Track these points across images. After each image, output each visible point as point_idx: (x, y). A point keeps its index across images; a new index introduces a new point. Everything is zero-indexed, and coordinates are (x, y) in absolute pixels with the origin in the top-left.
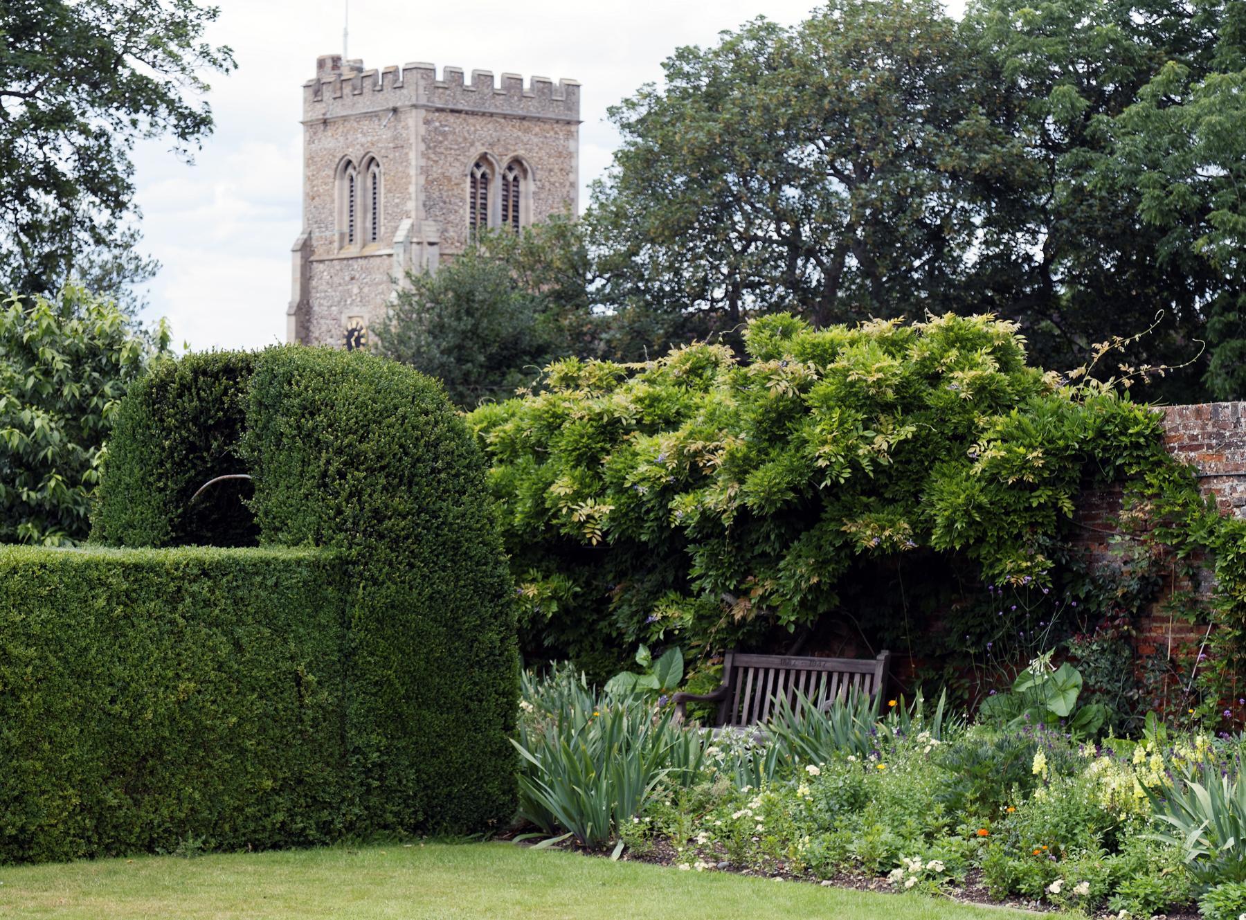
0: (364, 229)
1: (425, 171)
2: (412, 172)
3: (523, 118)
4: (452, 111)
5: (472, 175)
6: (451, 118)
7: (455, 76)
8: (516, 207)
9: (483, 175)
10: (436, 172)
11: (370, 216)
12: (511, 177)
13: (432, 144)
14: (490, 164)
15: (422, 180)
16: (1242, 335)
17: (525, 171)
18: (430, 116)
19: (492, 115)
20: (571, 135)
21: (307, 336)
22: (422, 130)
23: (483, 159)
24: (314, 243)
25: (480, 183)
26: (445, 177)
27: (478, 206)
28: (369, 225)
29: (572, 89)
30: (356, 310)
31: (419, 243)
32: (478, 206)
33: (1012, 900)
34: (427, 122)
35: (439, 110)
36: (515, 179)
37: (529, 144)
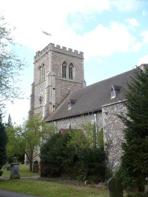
0: (43, 77)
1: (52, 62)
2: (50, 63)
3: (73, 56)
4: (58, 52)
5: (63, 66)
6: (58, 54)
7: (58, 46)
8: (72, 75)
9: (65, 66)
10: (55, 63)
11: (44, 75)
12: (71, 67)
13: (54, 58)
14: (66, 64)
15: (52, 64)
16: (147, 160)
17: (73, 66)
18: (53, 53)
19: (66, 55)
20: (82, 61)
21: (34, 100)
22: (52, 55)
23: (64, 63)
24: (35, 83)
25: (64, 68)
26: (57, 64)
27: (64, 72)
28: (43, 77)
29: (82, 53)
30: (41, 93)
31: (51, 76)
32: (64, 72)
33: (28, 122)
34: (53, 54)
35: (56, 52)
36: (71, 68)
37: (75, 61)
